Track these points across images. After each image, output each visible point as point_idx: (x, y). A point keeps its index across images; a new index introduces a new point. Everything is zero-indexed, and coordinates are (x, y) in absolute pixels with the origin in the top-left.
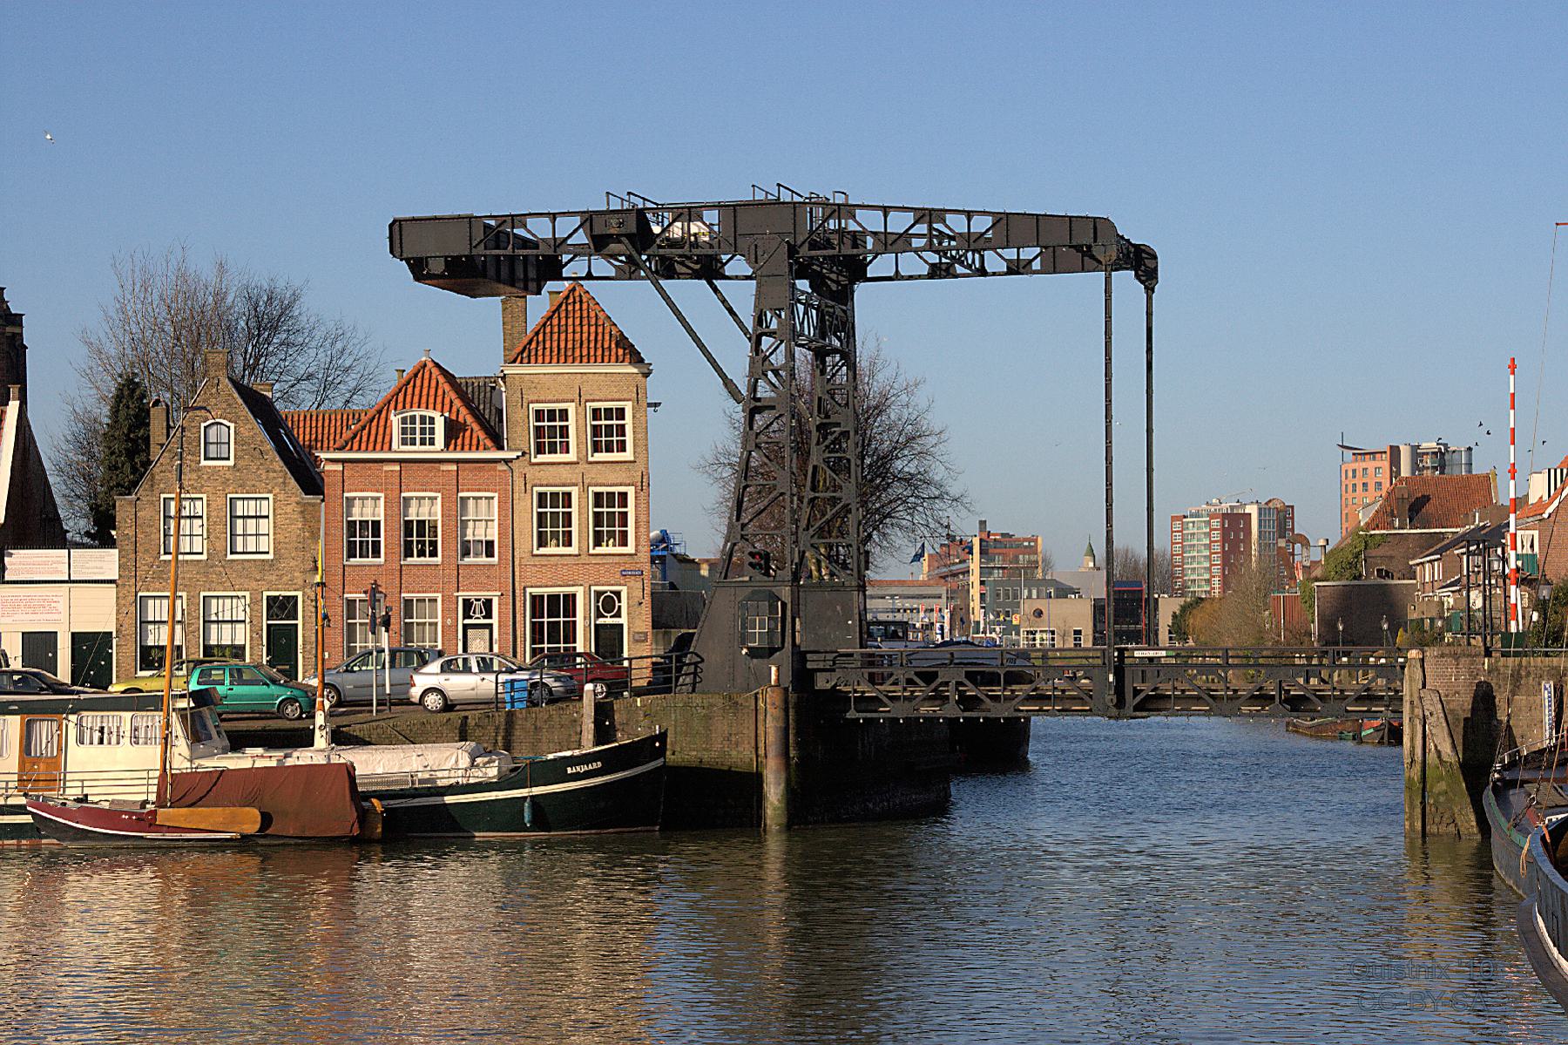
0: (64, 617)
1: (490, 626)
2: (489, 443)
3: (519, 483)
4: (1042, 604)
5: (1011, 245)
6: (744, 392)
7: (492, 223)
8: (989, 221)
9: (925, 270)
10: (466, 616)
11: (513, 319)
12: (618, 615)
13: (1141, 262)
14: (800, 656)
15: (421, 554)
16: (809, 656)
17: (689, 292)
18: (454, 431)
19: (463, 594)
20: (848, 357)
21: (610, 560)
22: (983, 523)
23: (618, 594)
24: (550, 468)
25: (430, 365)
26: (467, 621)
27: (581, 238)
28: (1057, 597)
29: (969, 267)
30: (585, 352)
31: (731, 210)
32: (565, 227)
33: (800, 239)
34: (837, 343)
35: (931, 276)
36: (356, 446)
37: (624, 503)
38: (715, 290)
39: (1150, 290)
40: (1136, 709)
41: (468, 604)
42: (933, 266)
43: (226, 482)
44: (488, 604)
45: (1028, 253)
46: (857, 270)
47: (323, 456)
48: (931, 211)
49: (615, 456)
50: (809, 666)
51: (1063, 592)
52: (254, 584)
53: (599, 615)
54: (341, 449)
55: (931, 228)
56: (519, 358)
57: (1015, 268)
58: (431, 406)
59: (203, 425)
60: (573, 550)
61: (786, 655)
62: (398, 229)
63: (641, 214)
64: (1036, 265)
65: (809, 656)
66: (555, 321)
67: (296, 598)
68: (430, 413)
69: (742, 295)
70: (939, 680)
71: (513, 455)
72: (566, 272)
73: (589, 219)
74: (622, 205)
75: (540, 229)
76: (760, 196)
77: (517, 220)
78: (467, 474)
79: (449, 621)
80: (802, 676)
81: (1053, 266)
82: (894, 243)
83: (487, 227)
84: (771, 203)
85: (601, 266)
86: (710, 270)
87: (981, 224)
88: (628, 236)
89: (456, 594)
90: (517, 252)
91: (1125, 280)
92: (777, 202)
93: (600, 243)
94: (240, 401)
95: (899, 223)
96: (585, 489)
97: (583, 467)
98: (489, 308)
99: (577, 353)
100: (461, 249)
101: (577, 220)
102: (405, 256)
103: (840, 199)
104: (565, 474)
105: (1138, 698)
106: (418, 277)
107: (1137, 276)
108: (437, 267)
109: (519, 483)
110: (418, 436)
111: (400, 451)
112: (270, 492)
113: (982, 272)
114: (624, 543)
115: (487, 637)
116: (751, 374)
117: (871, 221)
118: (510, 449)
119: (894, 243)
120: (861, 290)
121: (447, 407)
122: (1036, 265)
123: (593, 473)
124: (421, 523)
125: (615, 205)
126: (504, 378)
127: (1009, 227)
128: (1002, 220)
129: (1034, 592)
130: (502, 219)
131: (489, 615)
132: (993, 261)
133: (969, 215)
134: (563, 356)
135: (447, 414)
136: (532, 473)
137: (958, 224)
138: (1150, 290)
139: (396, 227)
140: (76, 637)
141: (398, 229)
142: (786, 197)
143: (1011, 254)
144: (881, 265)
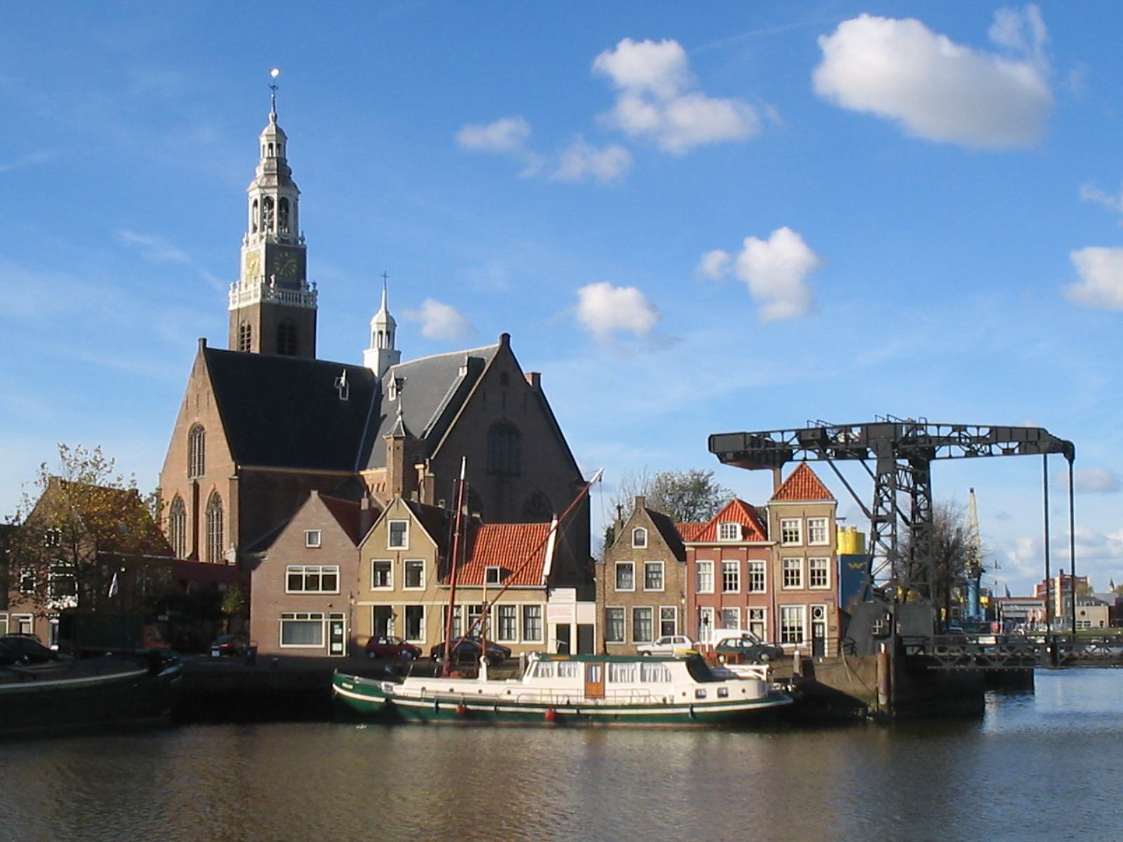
0: (574, 616)
1: (762, 623)
2: (762, 538)
3: (776, 556)
4: (1085, 609)
5: (1014, 439)
6: (871, 512)
7: (755, 435)
8: (987, 430)
9: (963, 454)
10: (752, 617)
11: (777, 478)
12: (822, 618)
13: (1067, 450)
14: (899, 639)
15: (731, 588)
16: (904, 639)
17: (850, 467)
18: (746, 532)
19: (749, 608)
20: (928, 497)
22: (1062, 571)
23: (822, 608)
24: (792, 549)
25: (736, 502)
26: (753, 621)
27: (795, 442)
28: (1096, 605)
29: (983, 452)
30: (807, 494)
31: (866, 427)
32: (788, 437)
33: (898, 440)
34: (921, 489)
35: (966, 456)
36: (701, 539)
38: (864, 463)
39: (1071, 462)
40: (1061, 665)
41: (752, 613)
42: (967, 452)
43: (643, 556)
44: (761, 613)
45: (1013, 445)
46: (932, 456)
47: (686, 544)
48: (960, 426)
49: (794, 544)
50: (904, 643)
51: (1098, 603)
52: (655, 603)
53: (813, 618)
54: (694, 541)
55: (960, 434)
56: (779, 496)
57: (1008, 452)
58: (736, 520)
59: (634, 530)
61: (892, 639)
62: (712, 439)
63: (823, 430)
64: (1017, 451)
65: (904, 639)
66: (793, 480)
67: (334, 588)
68: (733, 524)
69: (873, 464)
70: (1016, 650)
71: (772, 543)
72: (795, 458)
73: (799, 433)
74: (876, 419)
75: (777, 438)
76: (880, 420)
77: (767, 434)
78: (752, 552)
79: (743, 621)
80: (900, 648)
81: (1024, 451)
82: (948, 441)
83: (753, 437)
84: (884, 423)
85: (811, 455)
86: (863, 456)
87: (984, 432)
88: (817, 440)
89: (747, 608)
90: (767, 449)
91: (1057, 460)
92: (889, 423)
93: (804, 445)
94: (650, 519)
95: (945, 432)
96: (806, 559)
97: (805, 548)
98: (768, 474)
99: (803, 495)
100: (741, 448)
101: (793, 434)
102: (716, 451)
103: (923, 421)
105: (1063, 659)
106: (722, 462)
107: (1065, 456)
108: (730, 456)
110: (729, 534)
111: (720, 541)
112: (663, 560)
113: (990, 454)
115: (761, 629)
116: (875, 503)
117: (932, 432)
118: (772, 540)
119: (948, 441)
120: (933, 464)
121: (743, 521)
122: (1017, 451)
124: (819, 571)
125: (812, 426)
126: (769, 507)
127: (998, 434)
128: (993, 430)
129: (1081, 603)
130: (759, 434)
131: (762, 617)
132: (996, 449)
133: (978, 428)
134: (797, 497)
135: (743, 524)
136: (782, 552)
137: (973, 432)
138: (1071, 462)
139: (712, 440)
140: (579, 626)
141: (712, 439)
142: (892, 420)
143: (1004, 446)
144: (942, 451)
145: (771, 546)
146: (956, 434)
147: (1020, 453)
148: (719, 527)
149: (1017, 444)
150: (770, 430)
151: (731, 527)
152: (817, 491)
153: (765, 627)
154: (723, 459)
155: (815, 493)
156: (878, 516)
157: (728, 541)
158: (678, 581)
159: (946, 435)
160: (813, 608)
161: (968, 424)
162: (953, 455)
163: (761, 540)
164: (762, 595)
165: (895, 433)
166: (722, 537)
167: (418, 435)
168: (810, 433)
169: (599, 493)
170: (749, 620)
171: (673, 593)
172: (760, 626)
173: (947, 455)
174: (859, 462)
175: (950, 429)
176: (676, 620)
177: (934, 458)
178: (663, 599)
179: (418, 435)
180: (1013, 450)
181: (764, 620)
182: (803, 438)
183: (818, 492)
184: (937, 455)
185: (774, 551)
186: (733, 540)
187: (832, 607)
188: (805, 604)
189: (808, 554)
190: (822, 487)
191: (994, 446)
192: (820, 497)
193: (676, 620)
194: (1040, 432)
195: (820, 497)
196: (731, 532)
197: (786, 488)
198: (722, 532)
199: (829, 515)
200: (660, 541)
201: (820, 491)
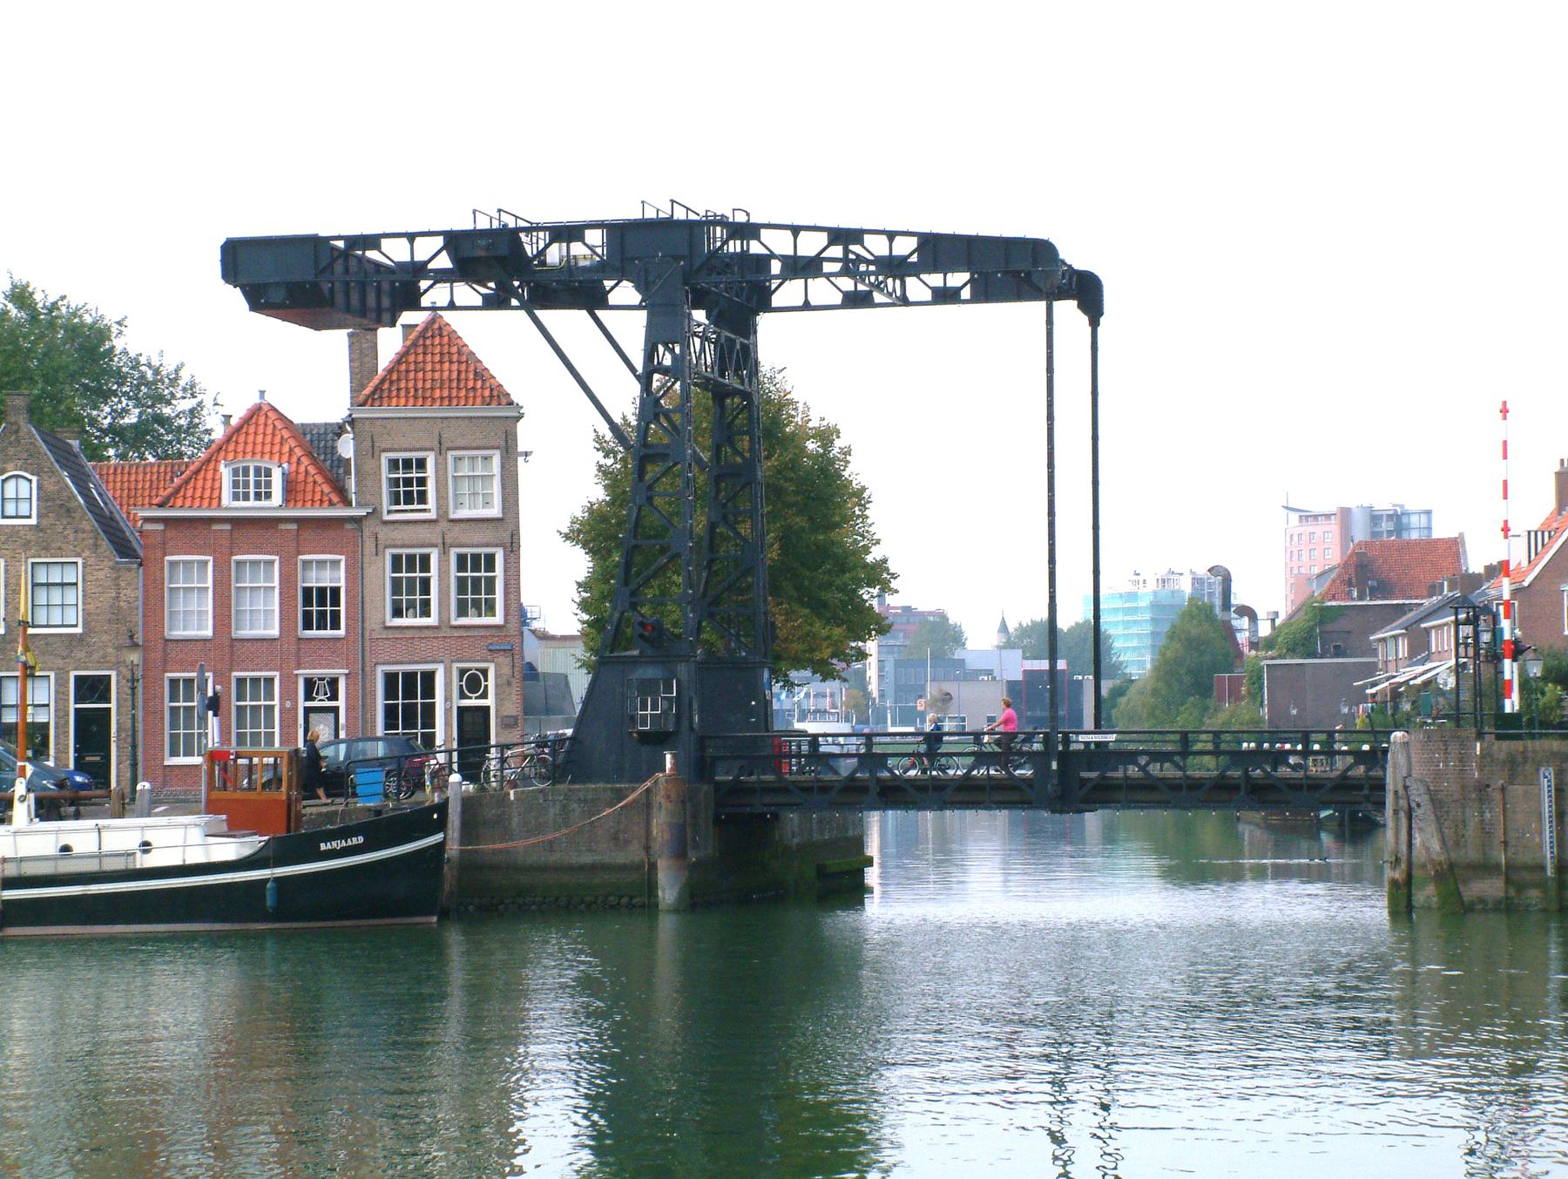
1: (335, 710)
2: (335, 499)
7: (341, 244)
8: (913, 243)
9: (837, 298)
10: (308, 697)
11: (362, 356)
12: (484, 696)
21: (409, 634)
23: (485, 672)
27: (444, 261)
37: (490, 566)
39: (1094, 324)
41: (310, 684)
42: (485, 297)
44: (333, 682)
45: (958, 279)
46: (763, 302)
52: (60, 662)
54: (161, 505)
57: (945, 296)
60: (432, 620)
64: (966, 294)
69: (631, 327)
71: (362, 512)
77: (373, 241)
81: (985, 292)
87: (904, 246)
96: (444, 552)
98: (335, 343)
101: (439, 241)
104: (424, 533)
108: (278, 295)
109: (369, 545)
110: (252, 490)
111: (229, 504)
112: (78, 555)
113: (904, 301)
114: (426, 612)
118: (359, 505)
120: (764, 321)
122: (966, 294)
123: (455, 533)
124: (322, 591)
131: (334, 697)
132: (917, 288)
136: (385, 534)
138: (1094, 324)
143: (936, 280)
144: (788, 293)
145: (357, 520)
146: (836, 251)
147: (977, 298)
148: (225, 473)
149: (966, 276)
150: (380, 231)
151: (258, 471)
152: (470, 384)
153: (342, 720)
154: (259, 300)
155: (467, 390)
156: (645, 445)
157: (251, 507)
158: (119, 608)
159: (812, 253)
160: (462, 672)
161: (865, 227)
162: (813, 302)
163: (331, 504)
164: (337, 639)
165: (691, 246)
166: (236, 497)
167: (1025, 625)
168: (483, 242)
169: (970, 886)
170: (302, 704)
171: (105, 637)
172: (331, 716)
173: (800, 303)
174: (584, 313)
175: (823, 238)
176: (113, 705)
177: (768, 308)
178: (80, 654)
179: (1025, 625)
180: (957, 291)
181: (341, 703)
182: (466, 254)
183: (474, 388)
184: (776, 301)
185: (367, 532)
186: (263, 503)
187: (506, 671)
188: (442, 662)
189: (448, 541)
190: (481, 374)
191: (911, 282)
192: (479, 400)
193: (113, 705)
194: (1041, 251)
195: (479, 400)
196: (258, 484)
197: (395, 377)
198: (236, 484)
199: (503, 443)
200: (72, 505)
201: (479, 384)
